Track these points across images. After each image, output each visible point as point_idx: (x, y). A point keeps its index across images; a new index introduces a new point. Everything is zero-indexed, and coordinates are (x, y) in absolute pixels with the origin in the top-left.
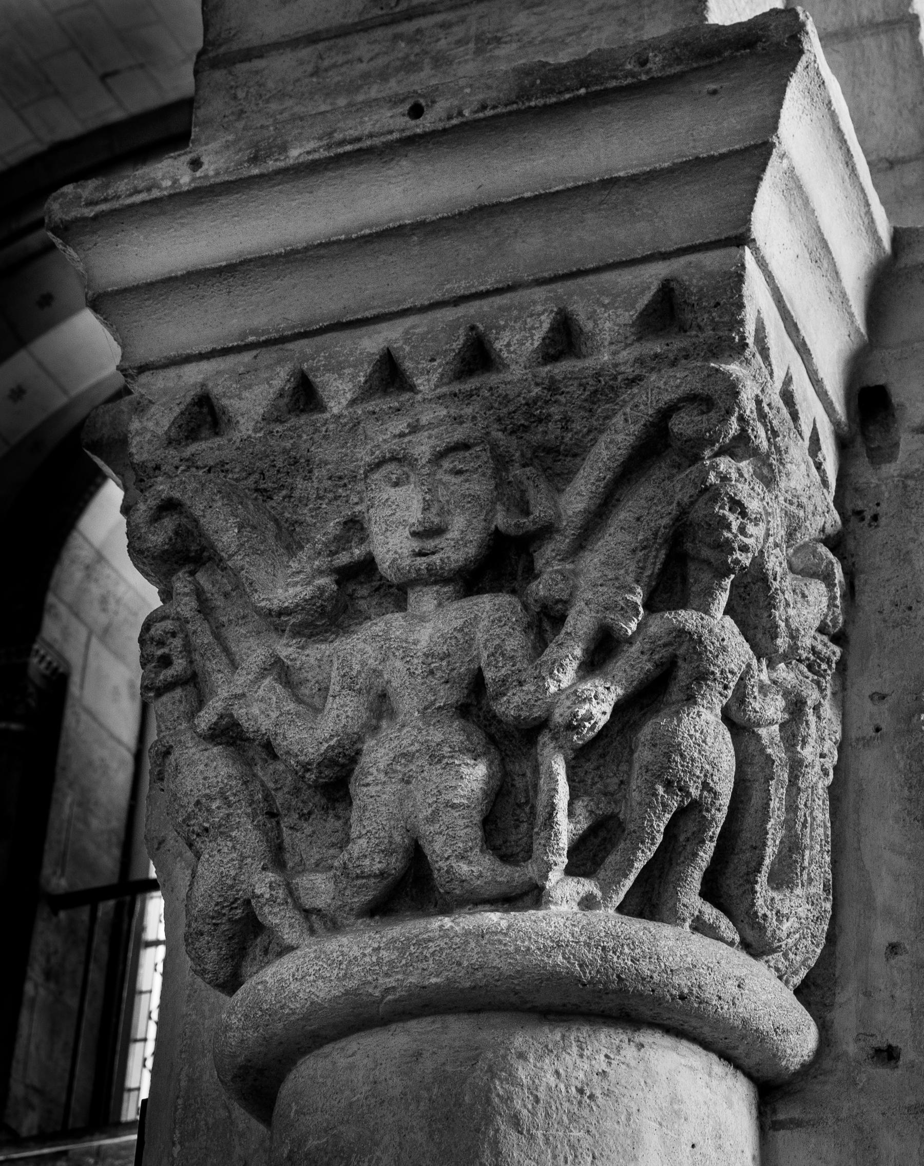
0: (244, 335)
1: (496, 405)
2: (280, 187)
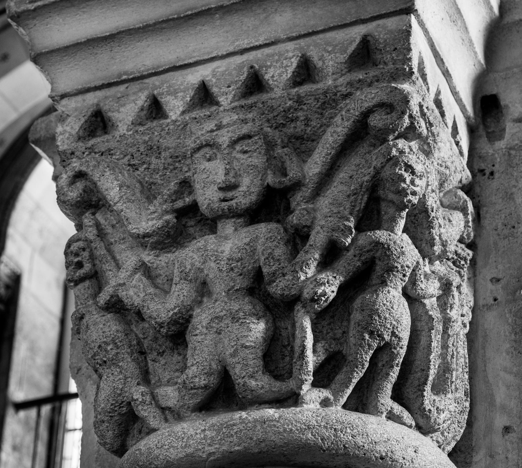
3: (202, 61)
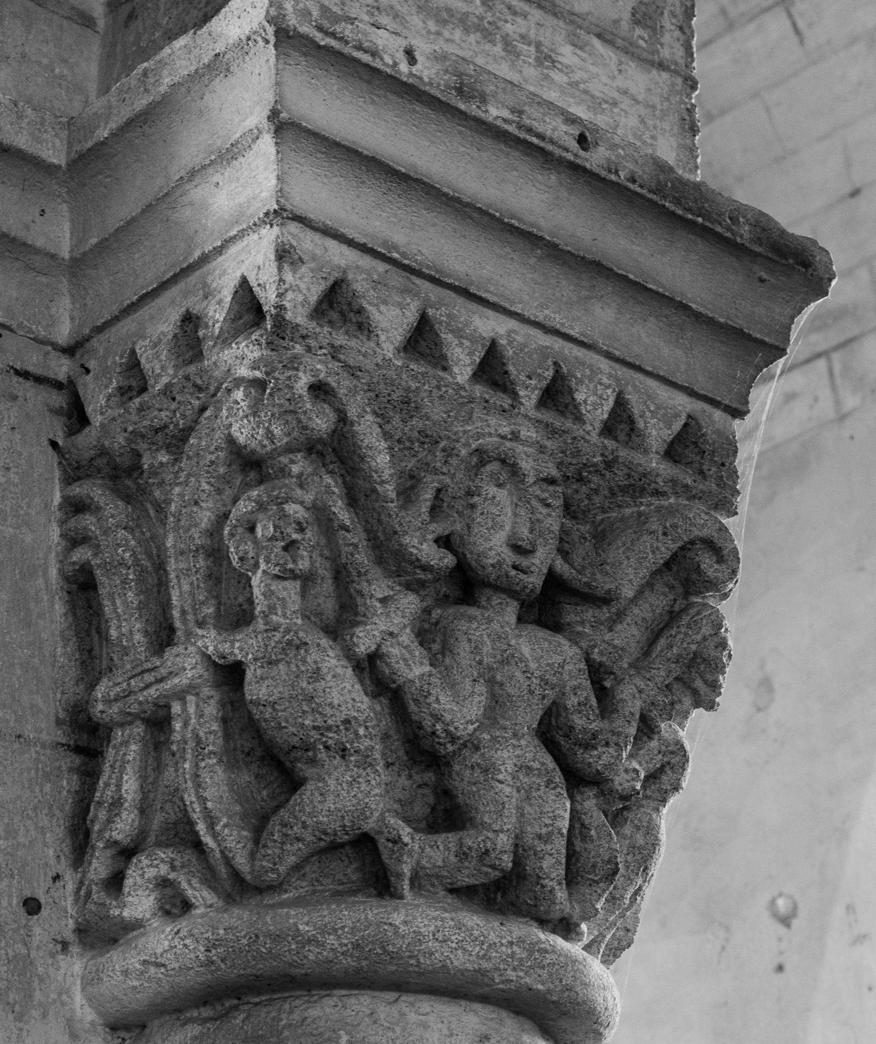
0: (385, 243)
1: (568, 452)
2: (463, 129)
3: (501, 307)
